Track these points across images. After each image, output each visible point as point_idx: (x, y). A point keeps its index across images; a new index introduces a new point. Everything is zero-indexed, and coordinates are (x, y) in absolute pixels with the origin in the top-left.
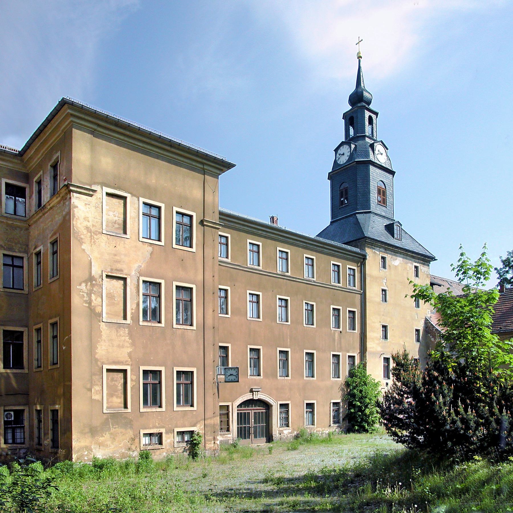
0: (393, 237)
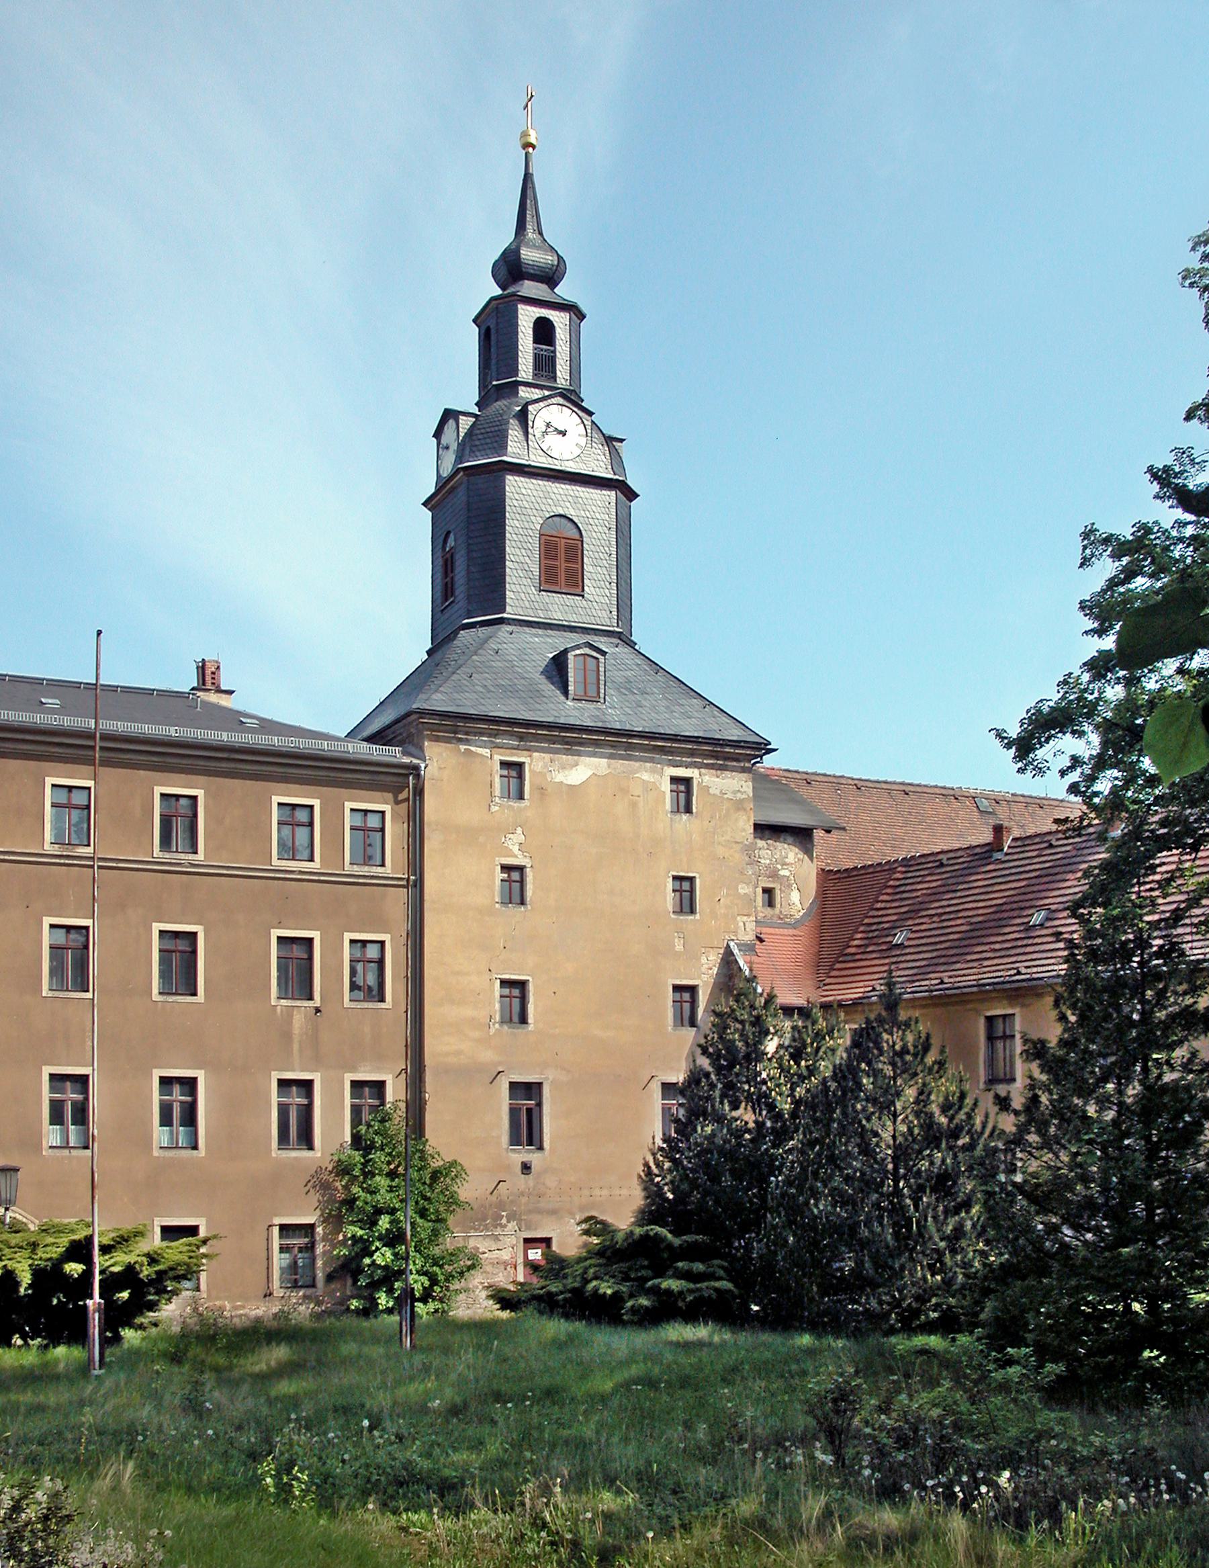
0: (566, 693)
